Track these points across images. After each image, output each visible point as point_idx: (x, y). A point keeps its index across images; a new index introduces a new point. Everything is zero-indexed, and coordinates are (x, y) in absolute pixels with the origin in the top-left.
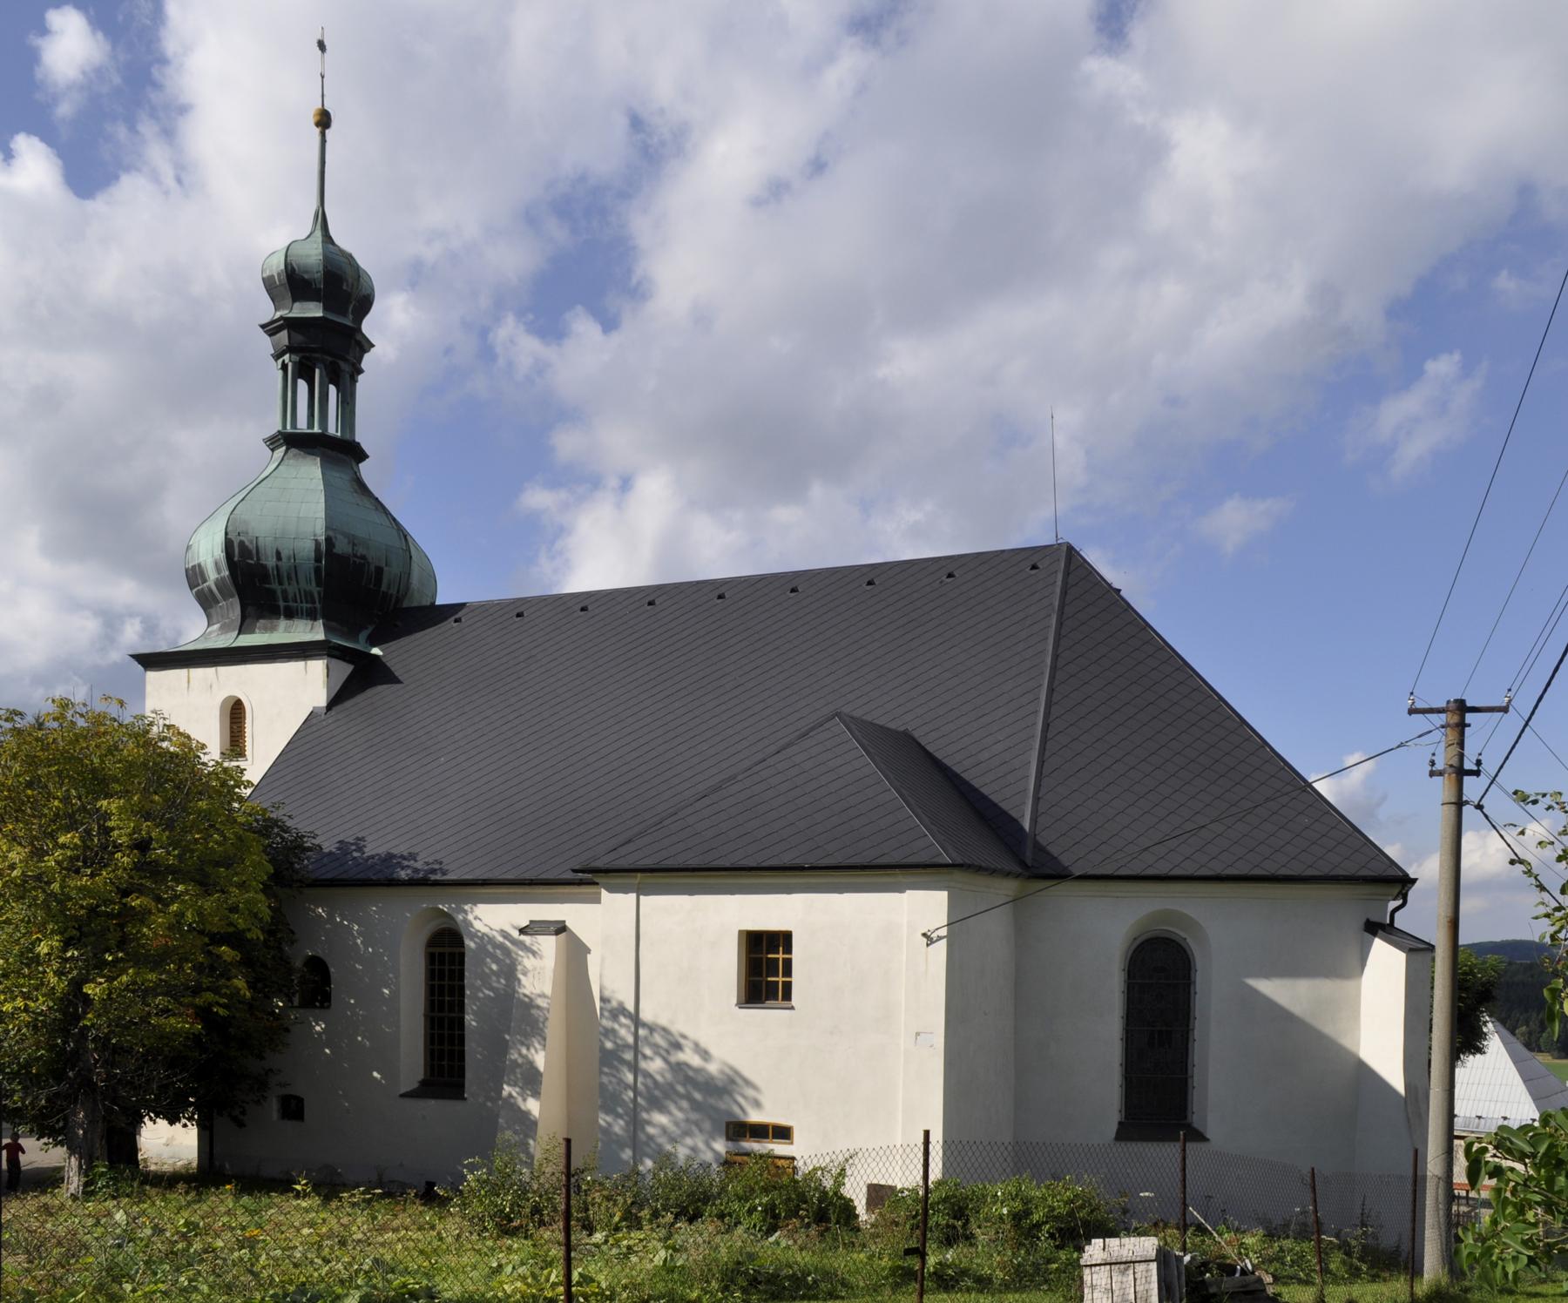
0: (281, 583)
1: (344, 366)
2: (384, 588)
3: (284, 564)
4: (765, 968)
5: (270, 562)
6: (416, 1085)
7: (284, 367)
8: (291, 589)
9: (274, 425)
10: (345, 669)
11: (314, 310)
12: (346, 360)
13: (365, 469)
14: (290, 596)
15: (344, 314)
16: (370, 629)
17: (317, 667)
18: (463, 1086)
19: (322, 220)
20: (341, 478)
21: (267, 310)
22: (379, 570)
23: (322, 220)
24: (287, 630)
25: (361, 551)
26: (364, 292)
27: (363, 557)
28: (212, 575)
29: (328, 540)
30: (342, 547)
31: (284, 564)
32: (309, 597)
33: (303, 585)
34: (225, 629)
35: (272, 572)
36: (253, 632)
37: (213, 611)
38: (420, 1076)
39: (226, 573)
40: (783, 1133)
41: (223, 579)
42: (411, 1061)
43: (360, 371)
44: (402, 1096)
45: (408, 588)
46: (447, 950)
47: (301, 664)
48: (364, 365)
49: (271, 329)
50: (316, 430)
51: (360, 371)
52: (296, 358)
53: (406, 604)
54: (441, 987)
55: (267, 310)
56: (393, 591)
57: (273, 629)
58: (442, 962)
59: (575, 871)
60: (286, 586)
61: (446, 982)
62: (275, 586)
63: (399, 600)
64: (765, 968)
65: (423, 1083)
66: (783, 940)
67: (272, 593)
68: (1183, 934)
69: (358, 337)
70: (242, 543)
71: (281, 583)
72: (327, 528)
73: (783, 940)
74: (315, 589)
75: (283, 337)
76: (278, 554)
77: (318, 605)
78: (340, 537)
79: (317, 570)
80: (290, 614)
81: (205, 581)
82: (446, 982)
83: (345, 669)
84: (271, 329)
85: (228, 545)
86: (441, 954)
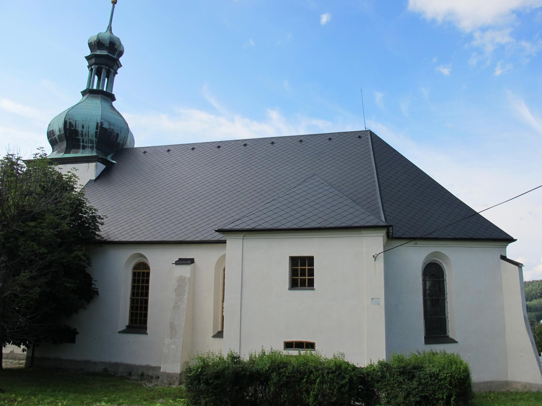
0: (82, 136)
1: (112, 70)
2: (118, 141)
3: (85, 130)
4: (302, 273)
5: (79, 129)
6: (125, 328)
7: (91, 70)
8: (86, 139)
9: (84, 88)
10: (102, 167)
11: (105, 53)
12: (113, 68)
13: (114, 103)
14: (85, 141)
15: (114, 55)
16: (112, 155)
17: (93, 165)
18: (146, 328)
19: (110, 28)
20: (106, 105)
21: (88, 53)
22: (118, 135)
23: (110, 28)
24: (82, 153)
25: (112, 127)
26: (122, 49)
27: (113, 130)
28: (57, 133)
29: (102, 123)
30: (106, 126)
31: (85, 130)
32: (92, 142)
33: (90, 137)
34: (59, 152)
35: (80, 132)
36: (70, 153)
37: (55, 147)
38: (127, 324)
39: (63, 132)
40: (311, 346)
41: (61, 135)
42: (123, 316)
43: (116, 73)
44: (119, 332)
45: (126, 142)
46: (141, 271)
47: (87, 164)
48: (118, 71)
49: (88, 58)
50: (100, 88)
51: (116, 73)
52: (97, 66)
53: (125, 147)
54: (138, 287)
55: (88, 53)
56: (121, 142)
57: (77, 153)
58: (139, 276)
59: (220, 231)
60: (84, 137)
61: (140, 285)
62: (80, 137)
63: (123, 146)
64: (302, 273)
65: (128, 327)
66: (310, 260)
67: (79, 140)
68: (441, 262)
69: (118, 62)
70: (70, 122)
71: (82, 136)
72: (101, 118)
73: (310, 260)
74: (94, 139)
75: (93, 61)
76: (83, 127)
77: (95, 145)
78: (106, 122)
79: (96, 133)
80: (84, 148)
81: (54, 135)
82: (140, 285)
83: (102, 167)
84: (88, 58)
85: (65, 122)
86: (139, 273)
